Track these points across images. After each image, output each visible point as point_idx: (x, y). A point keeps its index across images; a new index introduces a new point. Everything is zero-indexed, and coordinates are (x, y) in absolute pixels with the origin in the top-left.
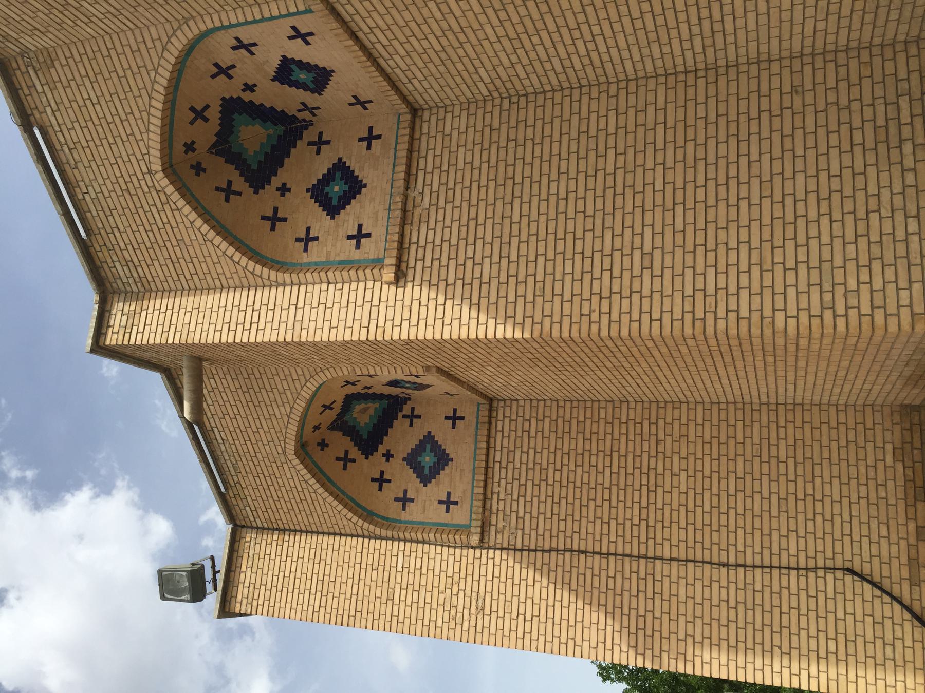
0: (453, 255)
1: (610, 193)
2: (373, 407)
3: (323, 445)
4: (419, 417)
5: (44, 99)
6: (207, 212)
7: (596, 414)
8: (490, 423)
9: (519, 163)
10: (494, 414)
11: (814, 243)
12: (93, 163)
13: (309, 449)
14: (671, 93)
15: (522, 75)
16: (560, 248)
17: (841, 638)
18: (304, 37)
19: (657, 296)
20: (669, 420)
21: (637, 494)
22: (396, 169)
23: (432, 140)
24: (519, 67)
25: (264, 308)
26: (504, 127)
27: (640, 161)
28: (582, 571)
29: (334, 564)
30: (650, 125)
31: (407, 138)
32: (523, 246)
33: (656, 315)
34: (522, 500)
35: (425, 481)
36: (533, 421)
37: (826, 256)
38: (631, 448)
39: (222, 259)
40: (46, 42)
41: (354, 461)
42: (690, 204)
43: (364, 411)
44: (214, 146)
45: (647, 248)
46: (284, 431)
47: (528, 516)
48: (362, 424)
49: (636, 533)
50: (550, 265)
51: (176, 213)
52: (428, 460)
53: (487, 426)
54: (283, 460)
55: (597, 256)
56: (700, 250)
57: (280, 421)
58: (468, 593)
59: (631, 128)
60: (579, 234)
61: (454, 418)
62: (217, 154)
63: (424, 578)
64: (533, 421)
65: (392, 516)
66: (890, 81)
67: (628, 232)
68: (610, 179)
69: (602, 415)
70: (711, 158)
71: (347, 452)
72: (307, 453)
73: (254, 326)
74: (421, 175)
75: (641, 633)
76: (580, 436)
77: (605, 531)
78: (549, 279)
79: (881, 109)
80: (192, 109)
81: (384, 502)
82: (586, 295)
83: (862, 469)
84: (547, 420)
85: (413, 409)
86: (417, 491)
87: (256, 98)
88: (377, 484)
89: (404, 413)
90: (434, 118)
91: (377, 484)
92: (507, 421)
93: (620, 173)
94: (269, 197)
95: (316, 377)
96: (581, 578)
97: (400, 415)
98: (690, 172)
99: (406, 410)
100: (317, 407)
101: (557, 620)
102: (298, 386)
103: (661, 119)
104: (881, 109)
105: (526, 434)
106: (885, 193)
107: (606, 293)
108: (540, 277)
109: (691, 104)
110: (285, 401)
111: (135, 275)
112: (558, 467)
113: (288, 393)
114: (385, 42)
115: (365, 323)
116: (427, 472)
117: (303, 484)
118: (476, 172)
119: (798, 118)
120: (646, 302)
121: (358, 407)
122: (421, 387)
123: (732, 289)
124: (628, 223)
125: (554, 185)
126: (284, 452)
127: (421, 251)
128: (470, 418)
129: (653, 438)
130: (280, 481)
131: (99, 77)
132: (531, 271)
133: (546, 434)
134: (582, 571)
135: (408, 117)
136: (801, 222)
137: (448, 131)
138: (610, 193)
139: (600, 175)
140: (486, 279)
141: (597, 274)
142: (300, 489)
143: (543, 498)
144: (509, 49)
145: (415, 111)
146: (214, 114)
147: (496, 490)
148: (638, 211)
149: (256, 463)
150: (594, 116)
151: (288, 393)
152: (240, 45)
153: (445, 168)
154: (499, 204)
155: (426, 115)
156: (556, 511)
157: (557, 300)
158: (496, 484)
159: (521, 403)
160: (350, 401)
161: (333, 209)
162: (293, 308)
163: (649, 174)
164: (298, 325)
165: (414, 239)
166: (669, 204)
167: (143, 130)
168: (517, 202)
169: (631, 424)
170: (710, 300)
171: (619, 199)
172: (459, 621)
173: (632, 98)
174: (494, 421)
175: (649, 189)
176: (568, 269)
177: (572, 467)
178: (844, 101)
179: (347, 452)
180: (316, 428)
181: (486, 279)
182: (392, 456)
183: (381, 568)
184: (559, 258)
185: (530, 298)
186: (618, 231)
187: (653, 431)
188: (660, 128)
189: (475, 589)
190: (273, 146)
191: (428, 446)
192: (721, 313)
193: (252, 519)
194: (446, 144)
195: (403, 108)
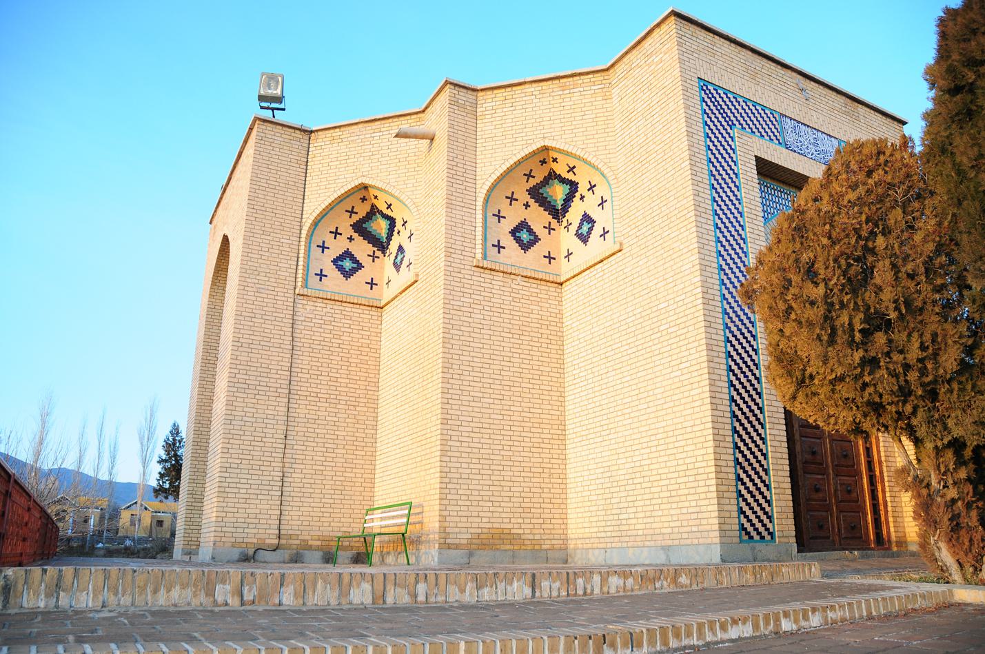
0: (486, 299)
1: (511, 384)
2: (383, 234)
5: (587, 89)
6: (520, 163)
8: (369, 306)
9: (530, 338)
10: (373, 309)
11: (480, 477)
12: (551, 106)
13: (363, 191)
14: (556, 417)
15: (574, 344)
16: (485, 356)
17: (247, 496)
18: (605, 233)
19: (460, 402)
20: (367, 414)
21: (325, 392)
22: (533, 272)
23: (545, 292)
24: (578, 342)
25: (464, 188)
26: (548, 332)
27: (525, 400)
28: (281, 355)
29: (285, 198)
30: (542, 406)
31: (548, 279)
32: (488, 337)
33: (450, 401)
34: (322, 322)
35: (335, 261)
36: (368, 333)
37: (474, 482)
38: (351, 390)
39: (493, 167)
40: (615, 100)
42: (502, 422)
44: (554, 172)
45: (483, 400)
47: (312, 325)
49: (302, 389)
50: (478, 350)
51: (521, 147)
52: (347, 264)
55: (481, 375)
56: (481, 425)
58: (267, 283)
59: (542, 397)
60: (492, 366)
62: (550, 172)
63: (276, 256)
64: (368, 333)
65: (314, 238)
66: (551, 516)
67: (491, 391)
68: (518, 384)
69: (371, 375)
70: (523, 434)
71: (356, 213)
72: (360, 189)
73: (454, 181)
74: (528, 284)
75: (246, 386)
77: (303, 371)
78: (471, 349)
79: (539, 511)
80: (574, 167)
81: (325, 236)
82: (462, 367)
83: (338, 515)
84: (369, 342)
85: (378, 257)
86: (330, 256)
87: (577, 199)
89: (376, 252)
90: (556, 294)
93: (520, 390)
94: (526, 197)
96: (277, 354)
97: (375, 249)
98: (518, 424)
99: (378, 253)
101: (252, 337)
102: (408, 194)
103: (515, 464)
104: (539, 511)
106: (501, 510)
107: (462, 377)
108: (472, 344)
109: (550, 426)
111: (487, 113)
112: (341, 346)
114: (597, 276)
116: (340, 263)
118: (527, 315)
119: (538, 475)
120: (457, 397)
122: (397, 266)
123: (461, 439)
124: (496, 392)
125: (517, 355)
127: (489, 281)
129: (357, 404)
131: (595, 124)
132: (475, 340)
133: (361, 340)
134: (281, 355)
135: (559, 281)
136: (490, 472)
137: (549, 301)
138: (511, 384)
139: (520, 380)
140: (473, 315)
141: (472, 374)
143: (323, 335)
144: (586, 338)
145: (561, 284)
146: (570, 176)
147: (328, 306)
148: (501, 397)
149: (357, 156)
150: (549, 379)
152: (603, 202)
153: (531, 298)
154: (510, 326)
155: (559, 290)
156: (315, 342)
157: (461, 352)
158: (331, 306)
160: (392, 222)
161: (514, 232)
162: (463, 205)
163: (519, 404)
165: (495, 278)
166: (503, 412)
167: (567, 140)
168: (511, 336)
169: (365, 392)
170: (456, 428)
171: (508, 388)
172: (251, 276)
173: (556, 398)
174: (370, 308)
175: (512, 403)
176: (475, 359)
177: (341, 354)
178: (543, 495)
179: (356, 213)
180: (376, 197)
181: (473, 315)
183: (282, 228)
184: (481, 355)
185: (462, 338)
186: (492, 386)
187: (361, 404)
188: (540, 411)
189: (270, 288)
190: (550, 202)
191: (355, 265)
192: (450, 432)
194: (543, 300)
195: (563, 279)
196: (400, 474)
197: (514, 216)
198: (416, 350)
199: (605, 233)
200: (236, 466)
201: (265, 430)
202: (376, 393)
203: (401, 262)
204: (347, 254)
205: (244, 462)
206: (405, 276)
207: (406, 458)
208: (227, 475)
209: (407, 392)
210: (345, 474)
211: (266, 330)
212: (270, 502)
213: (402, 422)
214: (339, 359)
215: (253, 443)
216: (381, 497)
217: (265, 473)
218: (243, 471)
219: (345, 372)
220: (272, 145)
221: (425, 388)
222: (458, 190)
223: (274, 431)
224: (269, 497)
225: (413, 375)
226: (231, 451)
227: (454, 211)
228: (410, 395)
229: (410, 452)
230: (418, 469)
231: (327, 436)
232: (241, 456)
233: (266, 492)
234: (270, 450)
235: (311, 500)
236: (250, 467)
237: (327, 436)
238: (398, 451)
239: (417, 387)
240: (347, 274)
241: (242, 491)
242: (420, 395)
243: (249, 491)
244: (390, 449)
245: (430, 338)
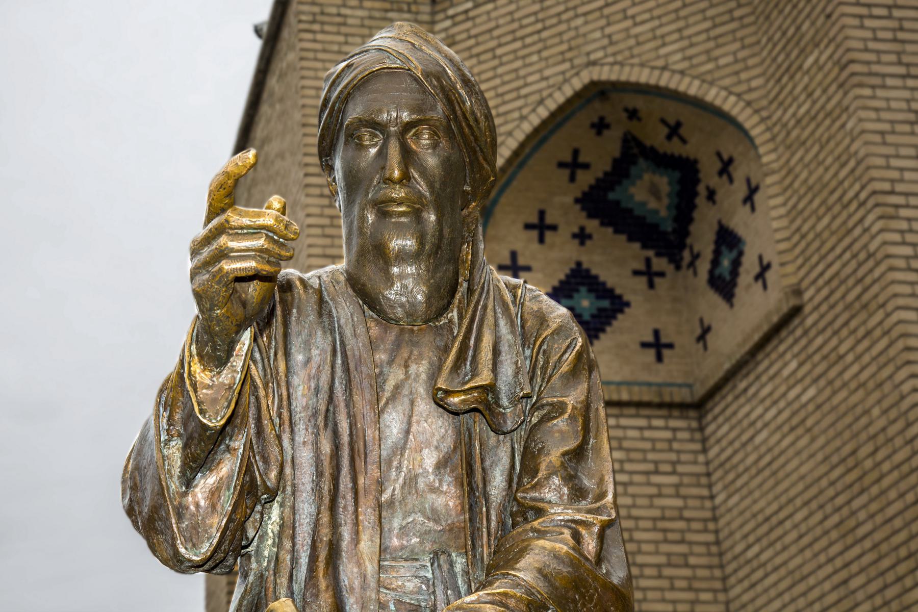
3: (600, 126)
4: (651, 285)
7: (704, 585)
10: (676, 413)
13: (597, 105)
18: (760, 276)
36: (674, 479)
41: (572, 179)
43: (655, 192)
46: (636, 61)
48: (633, 190)
53: (656, 400)
54: (577, 62)
57: (653, 55)
64: (674, 479)
72: (589, 101)
76: (662, 559)
84: (679, 503)
85: (662, 274)
88: (534, 219)
91: (534, 219)
92: (668, 434)
95: (749, 111)
97: (650, 253)
99: (660, 264)
100: (673, 111)
105: (650, 467)
110: (695, 61)
113: (710, 66)
115: (899, 187)
117: (536, 98)
121: (664, 182)
126: (594, 63)
128: (663, 373)
130: (535, 58)
133: (658, 502)
142: (524, 92)
146: (675, 148)
149: (564, 17)
151: (710, 66)
159: (701, 458)
164: (876, 81)
182: (582, 243)
191: (606, 304)
193: (451, 12)
198: (839, 501)
199: (765, 268)
220: (344, 30)
222: (881, 34)
225: (843, 574)
227: (880, 93)
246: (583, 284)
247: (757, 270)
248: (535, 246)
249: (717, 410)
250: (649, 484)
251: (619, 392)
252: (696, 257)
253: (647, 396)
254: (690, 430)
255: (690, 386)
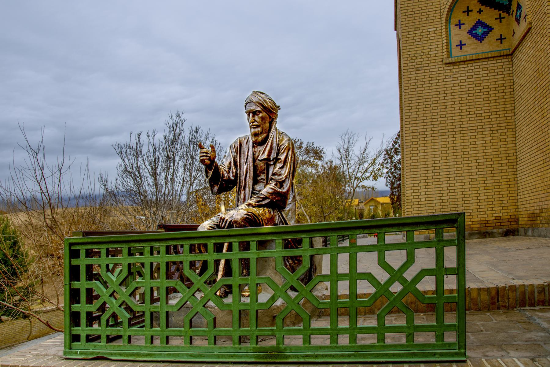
17: (426, 202)
21: (474, 125)
28: (439, 108)
35: (470, 32)
36: (503, 76)
52: (480, 31)
53: (499, 55)
61: (501, 39)
64: (503, 76)
81: (458, 15)
85: (504, 18)
89: (502, 14)
97: (501, 12)
116: (474, 32)
122: (518, 20)
128: (502, 47)
147: (469, 65)
191: (486, 30)
196: (532, 174)
197: (469, 22)
200: (417, 185)
201: (434, 159)
202: (513, 118)
203: (520, 17)
204: (479, 23)
205: (422, 181)
206: (524, 25)
207: (534, 162)
208: (412, 191)
209: (531, 114)
210: (494, 178)
211: (427, 94)
212: (442, 204)
213: (530, 136)
214: (482, 100)
215: (426, 169)
216: (521, 191)
217: (436, 186)
218: (422, 187)
219: (488, 108)
221: (542, 109)
223: (440, 159)
224: (441, 201)
226: (413, 176)
228: (534, 116)
229: (536, 157)
230: (542, 170)
231: (478, 155)
232: (419, 179)
233: (439, 198)
234: (439, 171)
235: (470, 199)
236: (426, 184)
237: (478, 155)
238: (529, 157)
239: (537, 109)
240: (480, 38)
241: (422, 200)
242: (540, 114)
243: (427, 199)
244: (524, 157)
245: (543, 70)
246: (479, 25)
247: (524, 16)
248: (466, 17)
249: (515, 56)
250: (495, 78)
251: (488, 54)
252: (513, 12)
253: (494, 54)
254: (509, 61)
255: (509, 49)
